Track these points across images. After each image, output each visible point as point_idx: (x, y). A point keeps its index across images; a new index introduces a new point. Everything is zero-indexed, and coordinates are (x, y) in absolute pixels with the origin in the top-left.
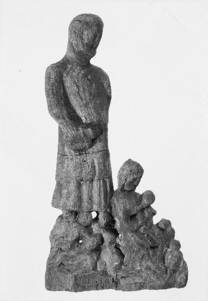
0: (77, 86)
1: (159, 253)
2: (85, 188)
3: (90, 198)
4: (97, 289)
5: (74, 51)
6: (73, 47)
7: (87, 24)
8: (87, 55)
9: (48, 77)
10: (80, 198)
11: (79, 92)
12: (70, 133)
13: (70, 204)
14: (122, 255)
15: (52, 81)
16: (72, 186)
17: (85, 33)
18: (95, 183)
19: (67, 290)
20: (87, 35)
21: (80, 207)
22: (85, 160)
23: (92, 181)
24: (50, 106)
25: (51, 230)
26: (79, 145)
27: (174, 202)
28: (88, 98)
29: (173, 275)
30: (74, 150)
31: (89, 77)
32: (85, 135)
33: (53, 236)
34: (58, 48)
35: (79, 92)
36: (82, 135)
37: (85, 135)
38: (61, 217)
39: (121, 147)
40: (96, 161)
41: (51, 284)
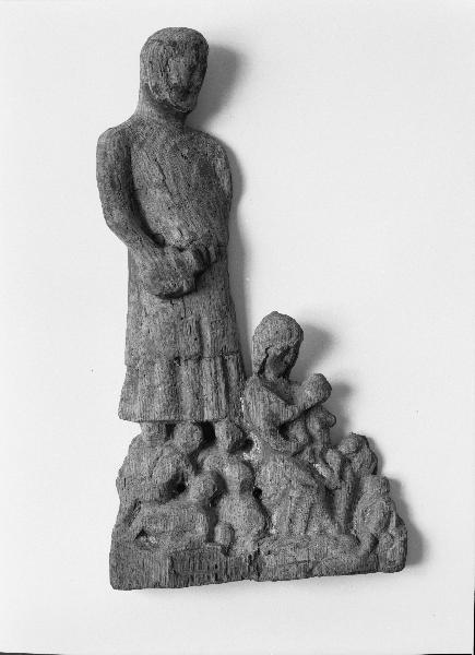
0: (161, 170)
1: (359, 521)
2: (185, 372)
3: (197, 395)
4: (218, 581)
5: (152, 100)
6: (150, 93)
7: (174, 44)
8: (177, 107)
9: (102, 154)
10: (175, 394)
11: (173, 168)
12: (148, 260)
13: (157, 409)
14: (265, 513)
15: (111, 160)
16: (159, 370)
17: (172, 63)
18: (205, 364)
19: (157, 585)
20: (178, 70)
21: (178, 410)
22: (183, 315)
23: (199, 358)
24: (108, 211)
25: (119, 467)
26: (169, 284)
27: (406, 414)
28: (183, 192)
29: (381, 541)
30: (159, 296)
31: (185, 151)
32: (180, 263)
33: (124, 482)
34: (121, 97)
35: (173, 168)
36: (174, 264)
37: (180, 263)
38: (137, 441)
39: (274, 287)
40: (205, 320)
41: (126, 573)
